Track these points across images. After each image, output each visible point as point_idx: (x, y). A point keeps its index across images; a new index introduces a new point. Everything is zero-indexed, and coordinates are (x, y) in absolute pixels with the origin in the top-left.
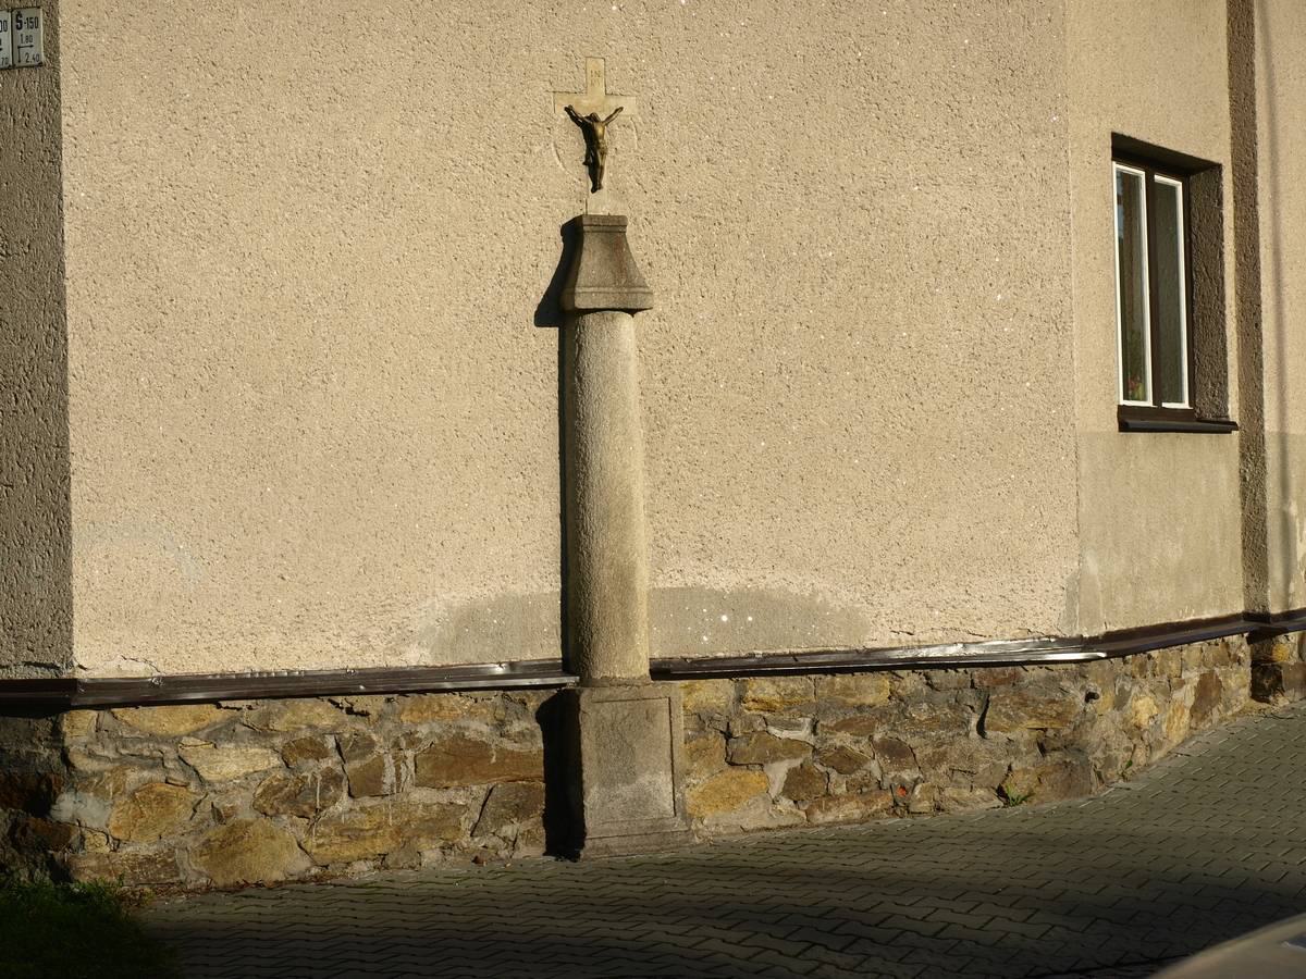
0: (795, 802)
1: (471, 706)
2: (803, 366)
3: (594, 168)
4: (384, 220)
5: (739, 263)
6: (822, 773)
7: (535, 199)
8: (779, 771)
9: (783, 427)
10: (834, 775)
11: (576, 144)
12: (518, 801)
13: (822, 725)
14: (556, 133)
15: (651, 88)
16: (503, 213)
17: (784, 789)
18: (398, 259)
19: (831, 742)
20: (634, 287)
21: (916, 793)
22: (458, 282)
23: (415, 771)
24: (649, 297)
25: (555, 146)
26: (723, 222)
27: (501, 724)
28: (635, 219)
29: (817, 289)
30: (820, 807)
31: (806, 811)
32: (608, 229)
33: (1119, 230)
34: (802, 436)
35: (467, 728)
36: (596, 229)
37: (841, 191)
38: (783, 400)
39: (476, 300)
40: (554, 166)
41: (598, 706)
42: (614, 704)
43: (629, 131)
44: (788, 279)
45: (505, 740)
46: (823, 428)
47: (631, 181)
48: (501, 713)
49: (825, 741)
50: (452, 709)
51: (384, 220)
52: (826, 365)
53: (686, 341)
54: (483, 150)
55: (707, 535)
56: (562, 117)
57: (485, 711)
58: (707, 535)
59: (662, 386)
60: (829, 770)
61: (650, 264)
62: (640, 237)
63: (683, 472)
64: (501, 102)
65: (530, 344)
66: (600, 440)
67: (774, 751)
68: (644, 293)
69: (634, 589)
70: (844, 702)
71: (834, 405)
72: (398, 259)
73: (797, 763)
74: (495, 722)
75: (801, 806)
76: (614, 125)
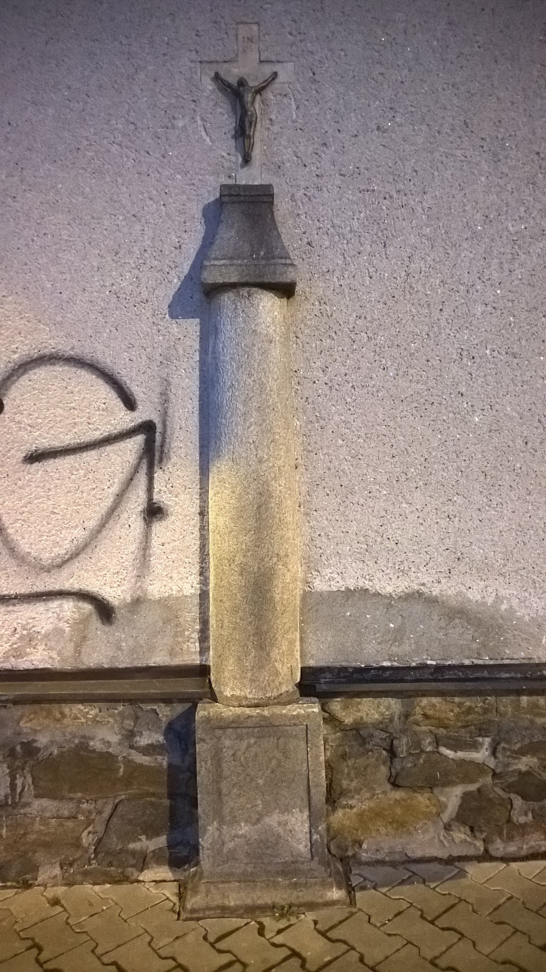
0: (472, 829)
1: (96, 715)
2: (488, 352)
3: (243, 132)
4: (12, 204)
5: (413, 240)
6: (503, 799)
7: (179, 177)
8: (453, 797)
9: (463, 420)
10: (518, 802)
11: (225, 119)
12: (146, 818)
13: (504, 748)
14: (203, 105)
15: (312, 53)
17: (458, 813)
18: (27, 245)
19: (515, 767)
20: (273, 258)
22: (93, 266)
24: (290, 269)
25: (203, 119)
26: (395, 195)
27: (131, 735)
28: (293, 196)
29: (506, 266)
30: (500, 835)
31: (484, 840)
33: (136, 694)
34: (485, 429)
36: (235, 199)
37: (536, 158)
38: (463, 390)
40: (201, 141)
41: (218, 732)
42: (239, 730)
43: (285, 100)
44: (472, 256)
45: (133, 751)
46: (512, 418)
47: (288, 154)
48: (129, 723)
49: (508, 765)
50: (76, 718)
51: (12, 204)
52: (516, 349)
53: (351, 327)
54: (120, 126)
56: (210, 88)
57: (111, 720)
58: (373, 535)
59: (321, 374)
60: (512, 796)
61: (309, 244)
62: (298, 215)
63: (345, 466)
64: (142, 75)
66: (233, 430)
67: (446, 774)
68: (286, 264)
69: (272, 598)
70: (532, 722)
71: (525, 393)
73: (473, 787)
74: (124, 732)
75: (478, 834)
76: (269, 94)
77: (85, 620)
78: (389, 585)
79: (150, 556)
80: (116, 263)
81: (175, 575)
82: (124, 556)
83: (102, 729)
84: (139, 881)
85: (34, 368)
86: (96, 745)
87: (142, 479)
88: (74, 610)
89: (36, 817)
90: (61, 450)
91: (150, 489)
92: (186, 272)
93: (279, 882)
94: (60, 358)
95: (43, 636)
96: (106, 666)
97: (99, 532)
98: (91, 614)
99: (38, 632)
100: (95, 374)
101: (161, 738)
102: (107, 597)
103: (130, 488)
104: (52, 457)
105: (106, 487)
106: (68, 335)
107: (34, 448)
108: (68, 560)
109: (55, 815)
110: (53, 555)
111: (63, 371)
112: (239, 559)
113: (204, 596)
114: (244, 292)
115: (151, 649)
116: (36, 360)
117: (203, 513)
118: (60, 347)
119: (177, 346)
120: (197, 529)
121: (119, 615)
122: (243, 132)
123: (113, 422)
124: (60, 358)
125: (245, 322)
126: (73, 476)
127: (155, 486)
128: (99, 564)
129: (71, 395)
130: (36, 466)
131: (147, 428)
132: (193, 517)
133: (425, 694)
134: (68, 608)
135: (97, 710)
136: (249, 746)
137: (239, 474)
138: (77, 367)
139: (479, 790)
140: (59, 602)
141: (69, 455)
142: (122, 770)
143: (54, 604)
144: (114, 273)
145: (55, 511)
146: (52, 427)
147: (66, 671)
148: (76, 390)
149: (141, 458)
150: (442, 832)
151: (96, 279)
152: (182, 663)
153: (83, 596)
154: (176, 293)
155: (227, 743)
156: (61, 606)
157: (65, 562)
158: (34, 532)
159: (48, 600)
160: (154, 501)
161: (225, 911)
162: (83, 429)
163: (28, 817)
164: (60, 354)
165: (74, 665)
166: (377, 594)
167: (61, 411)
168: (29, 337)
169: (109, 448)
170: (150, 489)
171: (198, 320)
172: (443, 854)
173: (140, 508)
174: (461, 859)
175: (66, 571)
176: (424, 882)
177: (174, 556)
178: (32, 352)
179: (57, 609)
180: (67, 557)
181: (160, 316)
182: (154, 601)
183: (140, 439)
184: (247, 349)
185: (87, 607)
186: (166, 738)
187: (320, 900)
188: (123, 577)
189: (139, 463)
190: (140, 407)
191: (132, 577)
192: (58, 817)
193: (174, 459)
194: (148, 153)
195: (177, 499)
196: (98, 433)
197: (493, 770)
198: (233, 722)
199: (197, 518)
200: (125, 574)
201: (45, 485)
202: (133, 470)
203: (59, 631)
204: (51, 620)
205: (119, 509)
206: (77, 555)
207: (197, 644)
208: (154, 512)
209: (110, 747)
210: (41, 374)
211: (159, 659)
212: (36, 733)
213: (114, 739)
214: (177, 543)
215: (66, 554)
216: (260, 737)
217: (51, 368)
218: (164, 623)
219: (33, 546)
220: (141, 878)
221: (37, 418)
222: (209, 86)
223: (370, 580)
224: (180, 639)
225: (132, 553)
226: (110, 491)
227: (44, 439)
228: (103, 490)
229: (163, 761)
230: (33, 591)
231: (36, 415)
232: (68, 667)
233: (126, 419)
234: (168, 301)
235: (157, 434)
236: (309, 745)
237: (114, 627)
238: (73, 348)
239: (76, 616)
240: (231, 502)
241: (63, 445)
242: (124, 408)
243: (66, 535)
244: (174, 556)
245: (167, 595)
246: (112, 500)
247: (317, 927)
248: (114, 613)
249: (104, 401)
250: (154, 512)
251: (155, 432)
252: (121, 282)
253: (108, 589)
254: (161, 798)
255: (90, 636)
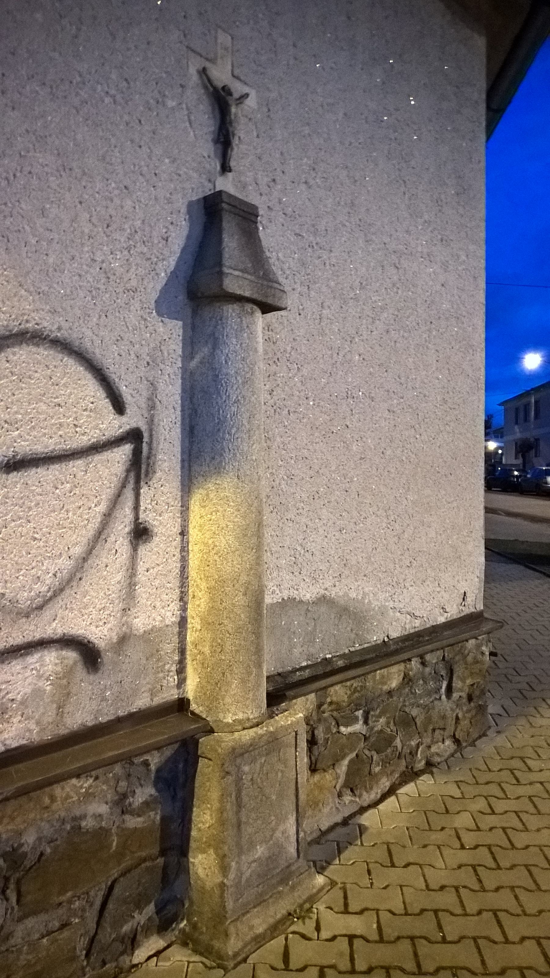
1: (90, 786)
3: (224, 140)
16: (134, 165)
21: (419, 755)
23: (18, 901)
32: (242, 213)
35: (83, 817)
36: (242, 213)
39: (103, 262)
45: (127, 817)
55: (299, 548)
65: (158, 330)
72: (7, 179)
77: (69, 673)
78: (308, 593)
79: (135, 585)
80: (108, 236)
81: (158, 604)
82: (111, 587)
83: (86, 800)
84: (136, 966)
85: (13, 345)
86: (88, 824)
87: (129, 494)
88: (57, 661)
89: (23, 947)
90: (44, 458)
91: (136, 508)
92: (172, 268)
93: (282, 891)
94: (45, 339)
95: (8, 705)
96: (90, 724)
97: (85, 560)
98: (75, 663)
99: (13, 700)
100: (82, 366)
101: (153, 791)
102: (93, 639)
103: (118, 507)
104: (34, 466)
105: (93, 505)
106: (54, 312)
107: (11, 454)
108: (51, 599)
109: (45, 932)
110: (32, 593)
111: (47, 356)
112: (244, 578)
113: (183, 622)
114: (249, 307)
115: (135, 692)
116: (16, 335)
117: (183, 533)
118: (45, 324)
119: (162, 348)
120: (178, 550)
121: (107, 657)
122: (224, 140)
123: (101, 426)
124: (45, 339)
125: (249, 338)
126: (58, 491)
127: (141, 504)
128: (85, 600)
129: (57, 387)
130: (14, 476)
131: (134, 436)
132: (174, 537)
133: (332, 685)
134: (50, 660)
135: (91, 781)
136: (262, 766)
137: (244, 492)
138: (63, 353)
139: (357, 755)
140: (39, 655)
141: (53, 463)
142: (115, 844)
143: (33, 659)
144: (105, 248)
145: (36, 536)
146: (33, 428)
147: (46, 742)
148: (63, 382)
149: (128, 471)
150: (337, 800)
151: (86, 249)
152: (162, 701)
153: (68, 642)
154: (163, 288)
155: (246, 768)
156: (41, 659)
157: (47, 602)
158: (9, 565)
159: (27, 654)
160: (140, 521)
161: (260, 941)
162: (69, 433)
163: (13, 952)
164: (45, 334)
165: (56, 732)
166: (301, 602)
167: (44, 407)
168: (7, 303)
169: (97, 458)
170: (136, 508)
171: (180, 323)
172: (338, 818)
173: (127, 530)
174: (353, 816)
175: (47, 613)
176: (351, 844)
177: (157, 583)
178: (12, 324)
179: (37, 665)
180: (49, 594)
181: (148, 310)
182: (139, 636)
183: (127, 448)
184: (251, 366)
185: (71, 655)
186: (158, 790)
187: (315, 891)
188: (108, 612)
189: (127, 476)
190: (128, 411)
191: (118, 611)
192: (49, 933)
193: (159, 474)
194: (140, 121)
195: (161, 518)
196: (85, 438)
197: (364, 735)
198: (251, 745)
199: (179, 539)
200: (111, 609)
201: (24, 503)
202: (120, 485)
203: (38, 692)
204: (29, 680)
205: (106, 531)
206: (62, 590)
207: (176, 677)
208: (141, 533)
209: (102, 820)
210: (22, 355)
211: (142, 702)
212: (21, 834)
213: (104, 809)
214: (160, 568)
215: (48, 592)
216: (267, 754)
217: (34, 349)
218: (147, 659)
219: (9, 585)
220: (135, 961)
221: (16, 413)
222: (195, 78)
223: (297, 590)
224: (161, 675)
225: (119, 582)
226: (97, 509)
227: (24, 441)
228: (90, 508)
229: (156, 816)
230: (8, 645)
231: (15, 408)
232: (48, 737)
233: (113, 425)
234: (155, 296)
235: (144, 445)
236: (298, 749)
237: (99, 674)
238: (59, 329)
239: (59, 669)
240: (236, 520)
241: (46, 451)
242: (113, 411)
243: (50, 567)
244: (157, 583)
245: (151, 626)
246: (99, 520)
247: (336, 910)
248: (100, 657)
249: (91, 400)
250: (141, 533)
251: (142, 442)
252: (112, 261)
253: (93, 628)
254: (153, 860)
255: (74, 691)
